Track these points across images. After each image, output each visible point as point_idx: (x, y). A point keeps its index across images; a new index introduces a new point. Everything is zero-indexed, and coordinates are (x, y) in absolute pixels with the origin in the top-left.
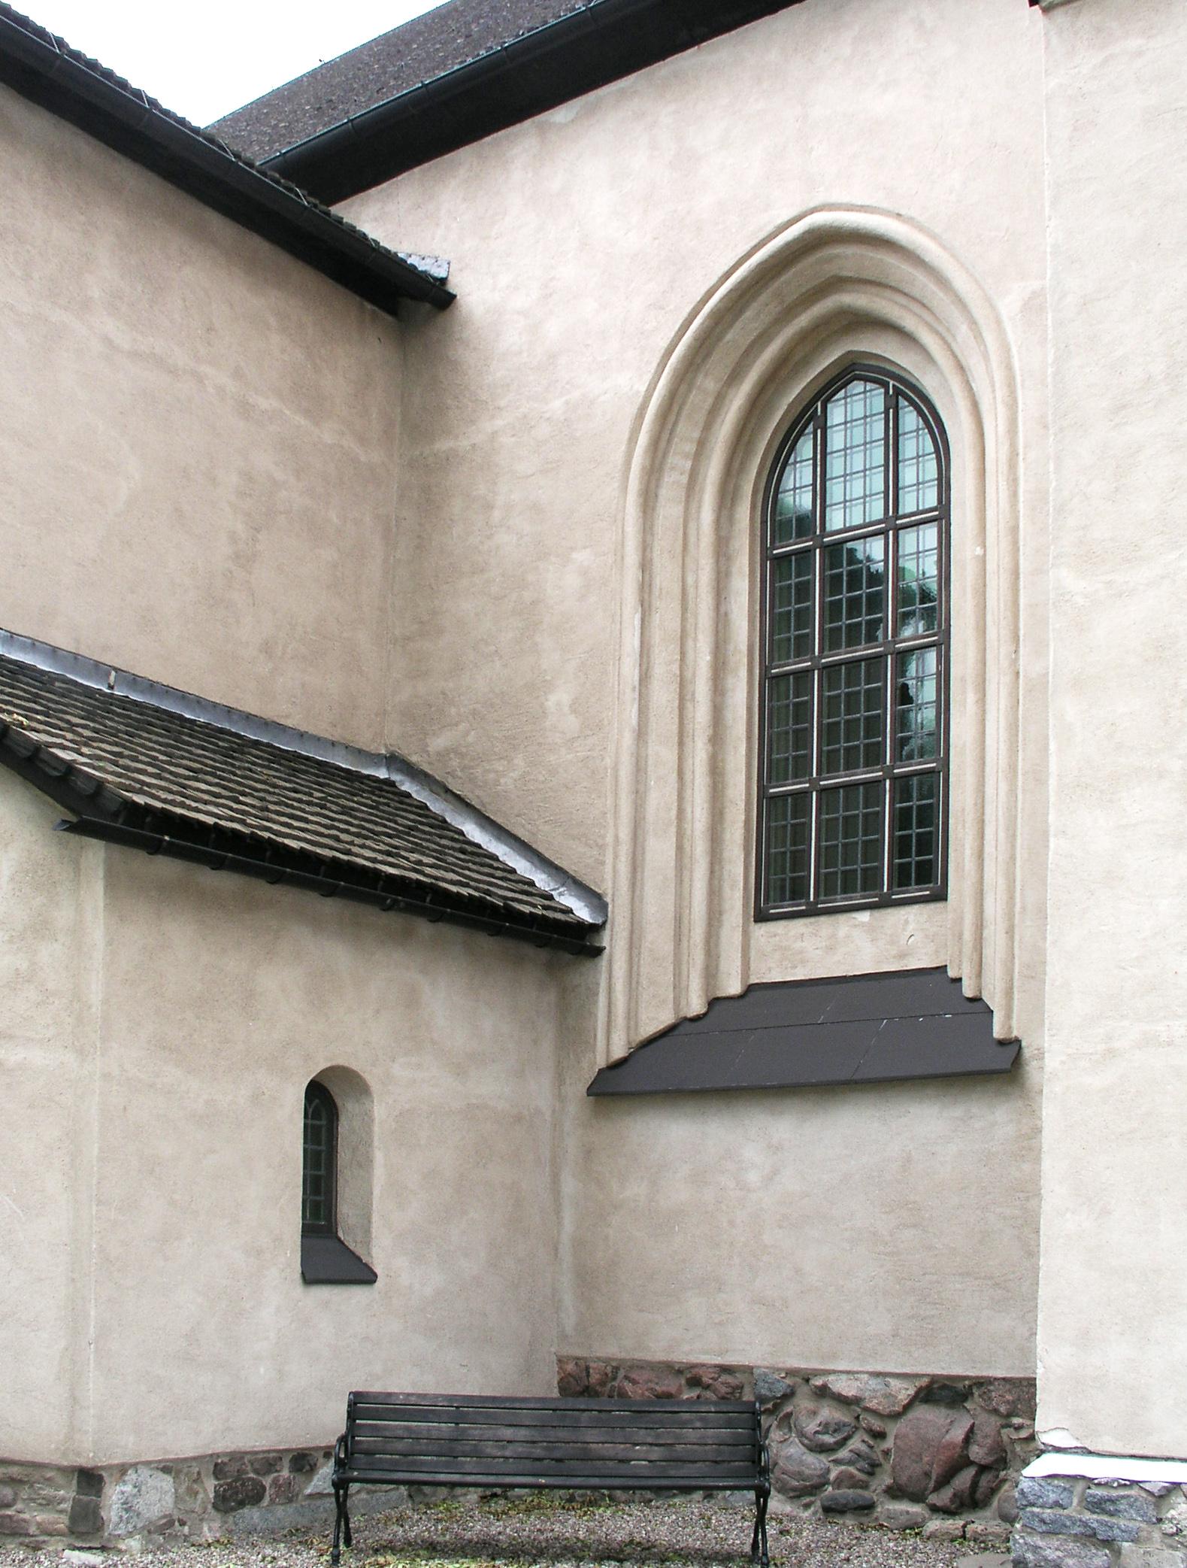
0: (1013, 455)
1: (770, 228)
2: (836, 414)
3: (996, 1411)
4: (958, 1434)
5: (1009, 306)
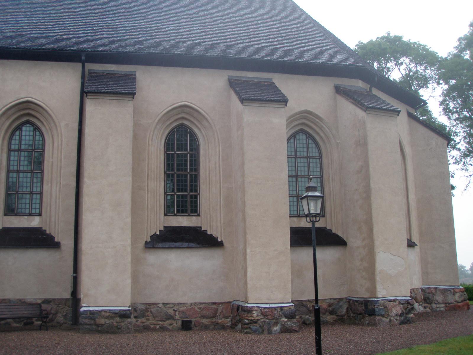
0: (61, 148)
1: (20, 98)
2: (24, 128)
3: (56, 304)
4: (49, 309)
5: (63, 124)
